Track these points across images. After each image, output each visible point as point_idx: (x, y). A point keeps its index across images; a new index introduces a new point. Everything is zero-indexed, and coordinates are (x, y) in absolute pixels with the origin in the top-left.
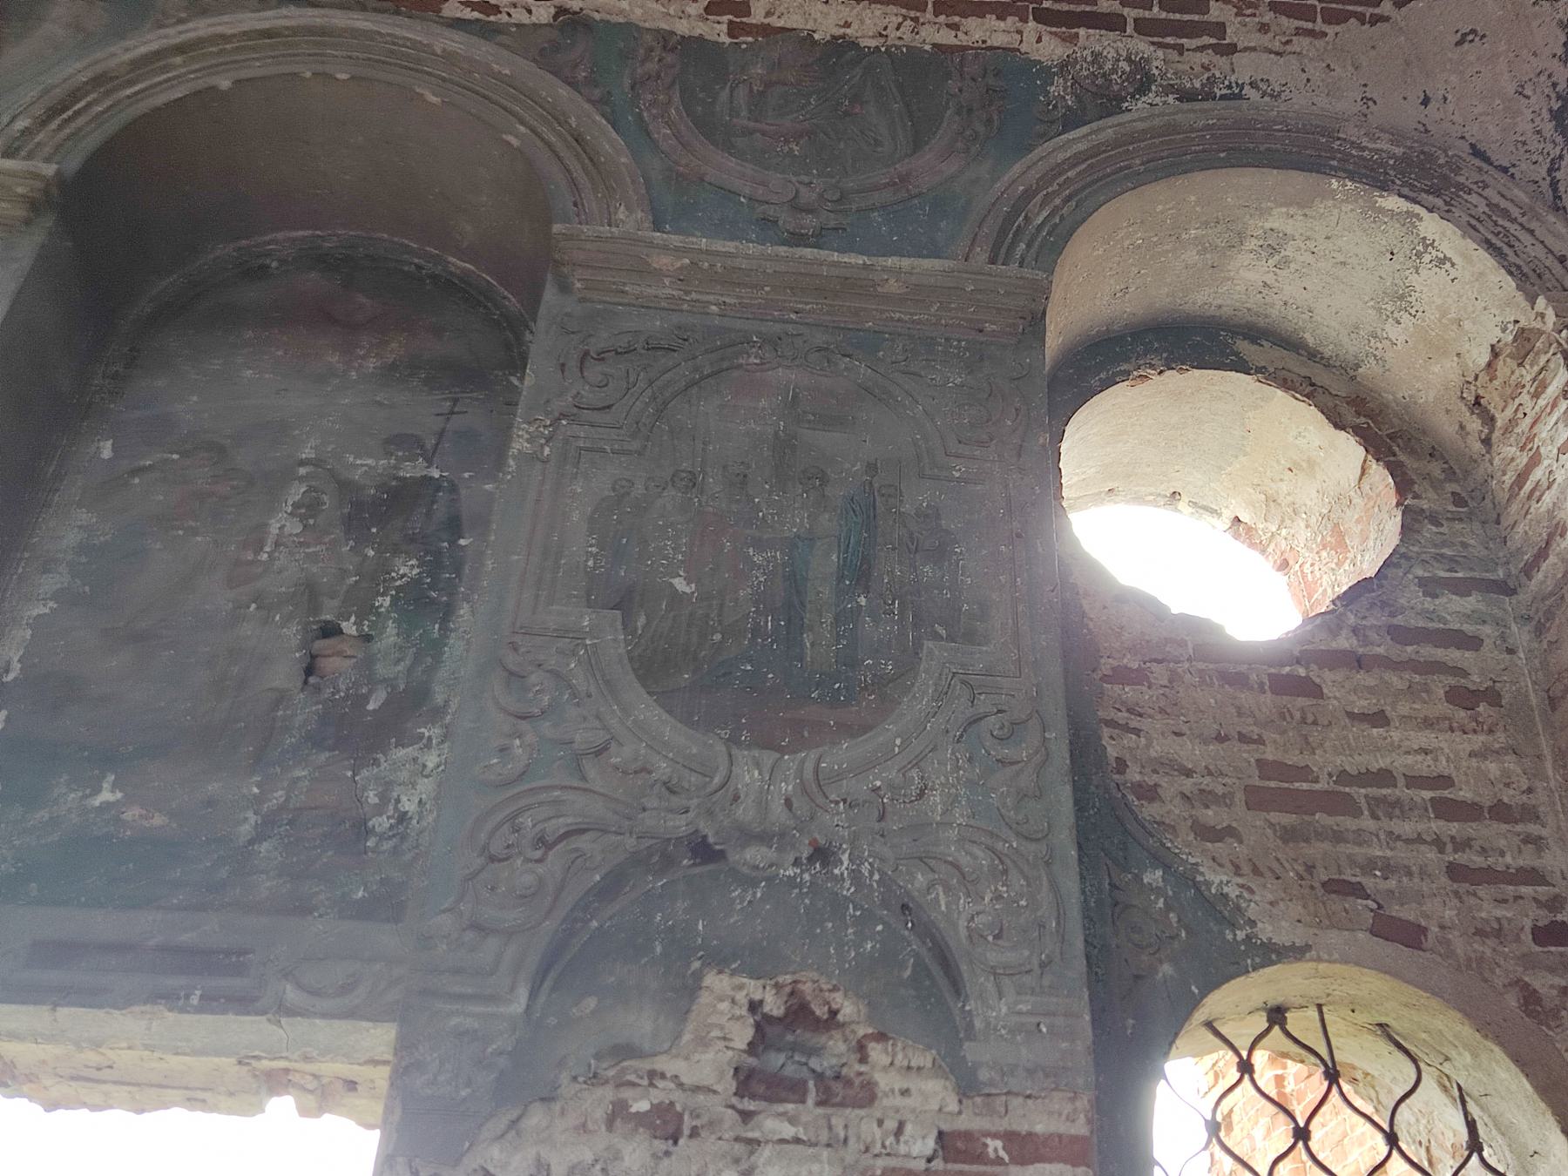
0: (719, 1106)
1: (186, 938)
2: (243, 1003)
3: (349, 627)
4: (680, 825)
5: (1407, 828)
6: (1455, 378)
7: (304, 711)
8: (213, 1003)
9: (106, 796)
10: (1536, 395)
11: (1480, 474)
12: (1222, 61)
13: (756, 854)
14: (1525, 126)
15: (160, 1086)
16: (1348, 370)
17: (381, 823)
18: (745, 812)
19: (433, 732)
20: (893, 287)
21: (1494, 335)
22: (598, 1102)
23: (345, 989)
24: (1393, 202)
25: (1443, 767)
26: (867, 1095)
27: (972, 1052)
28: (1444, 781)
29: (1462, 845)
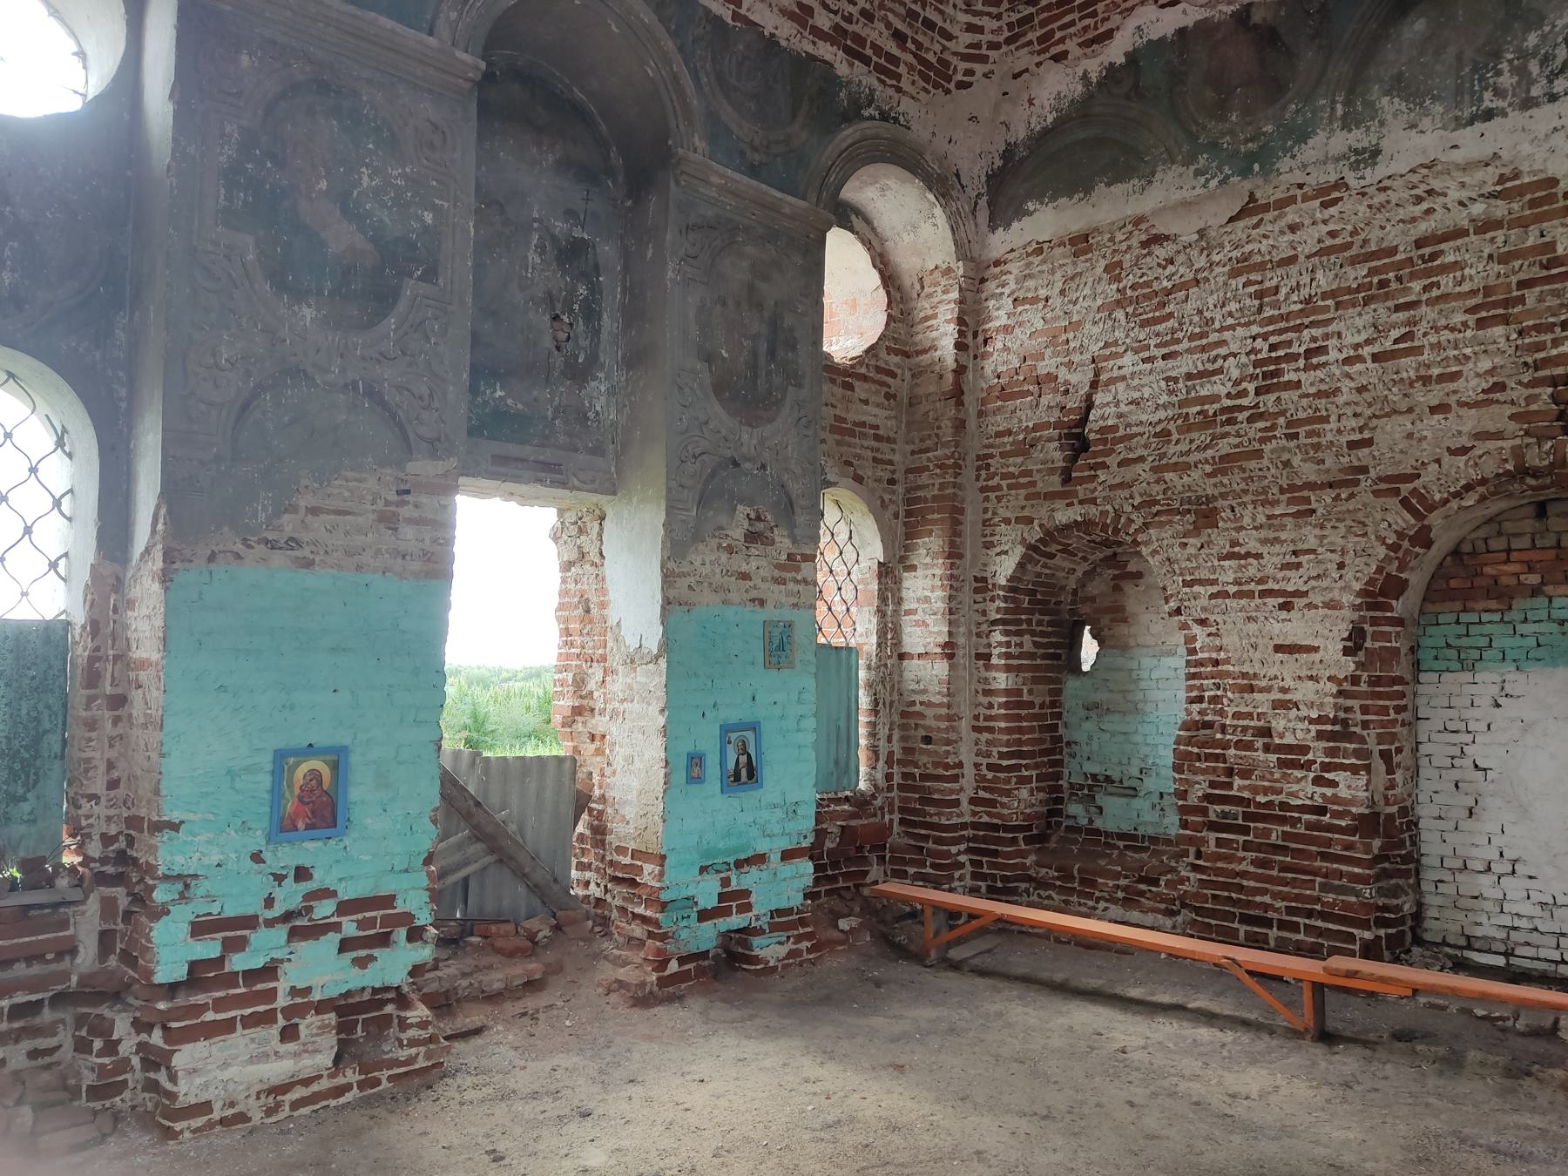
0: (741, 544)
1: (541, 458)
2: (563, 485)
3: (565, 318)
4: (728, 453)
5: (866, 443)
6: (919, 267)
7: (558, 360)
8: (555, 484)
9: (499, 393)
10: (944, 292)
11: (913, 304)
12: (896, 96)
13: (747, 465)
14: (976, 171)
15: (245, 407)
16: (882, 241)
17: (591, 415)
18: (744, 449)
19: (601, 375)
20: (787, 210)
21: (939, 263)
22: (714, 542)
23: (593, 481)
24: (931, 197)
25: (878, 422)
26: (773, 543)
27: (796, 531)
28: (877, 427)
29: (877, 450)
